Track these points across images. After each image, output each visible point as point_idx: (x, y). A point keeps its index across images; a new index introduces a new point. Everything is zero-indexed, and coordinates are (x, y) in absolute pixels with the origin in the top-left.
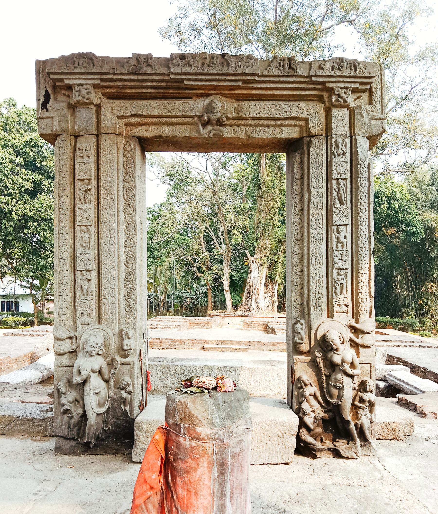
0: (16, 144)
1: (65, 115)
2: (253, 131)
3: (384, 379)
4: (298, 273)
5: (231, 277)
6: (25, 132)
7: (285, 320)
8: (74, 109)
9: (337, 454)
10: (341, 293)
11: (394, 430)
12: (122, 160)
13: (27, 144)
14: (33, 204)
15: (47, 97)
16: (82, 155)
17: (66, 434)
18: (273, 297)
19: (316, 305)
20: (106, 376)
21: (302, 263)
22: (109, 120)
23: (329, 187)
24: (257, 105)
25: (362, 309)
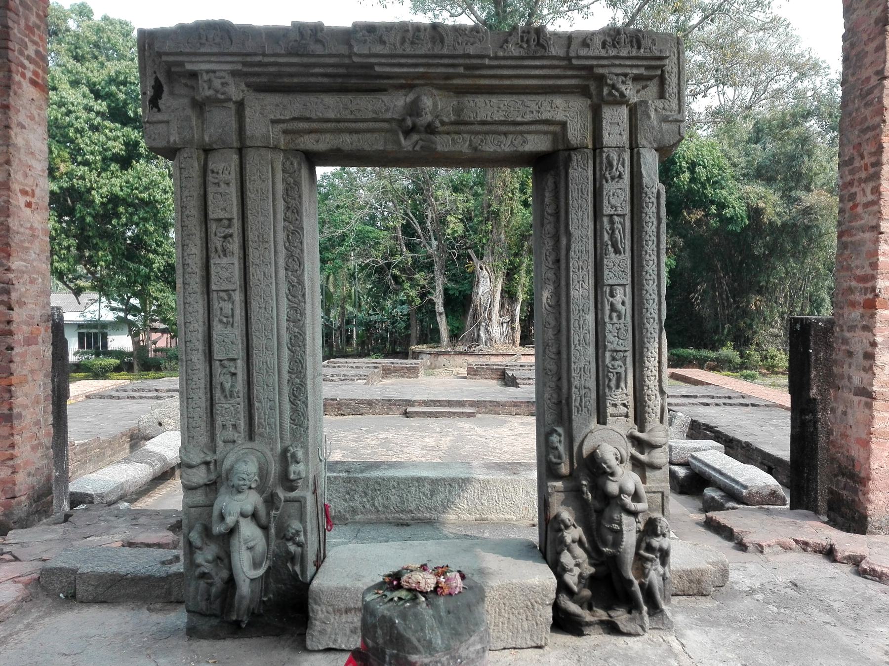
0: (94, 79)
1: (188, 119)
2: (482, 141)
3: (686, 465)
4: (553, 356)
5: (446, 291)
6: (108, 60)
7: (532, 359)
8: (201, 107)
9: (612, 628)
10: (618, 387)
11: (699, 582)
12: (280, 187)
13: (112, 81)
14: (125, 177)
15: (158, 89)
16: (216, 181)
17: (204, 609)
18: (512, 323)
19: (580, 405)
22: (258, 125)
23: (598, 227)
24: (488, 102)
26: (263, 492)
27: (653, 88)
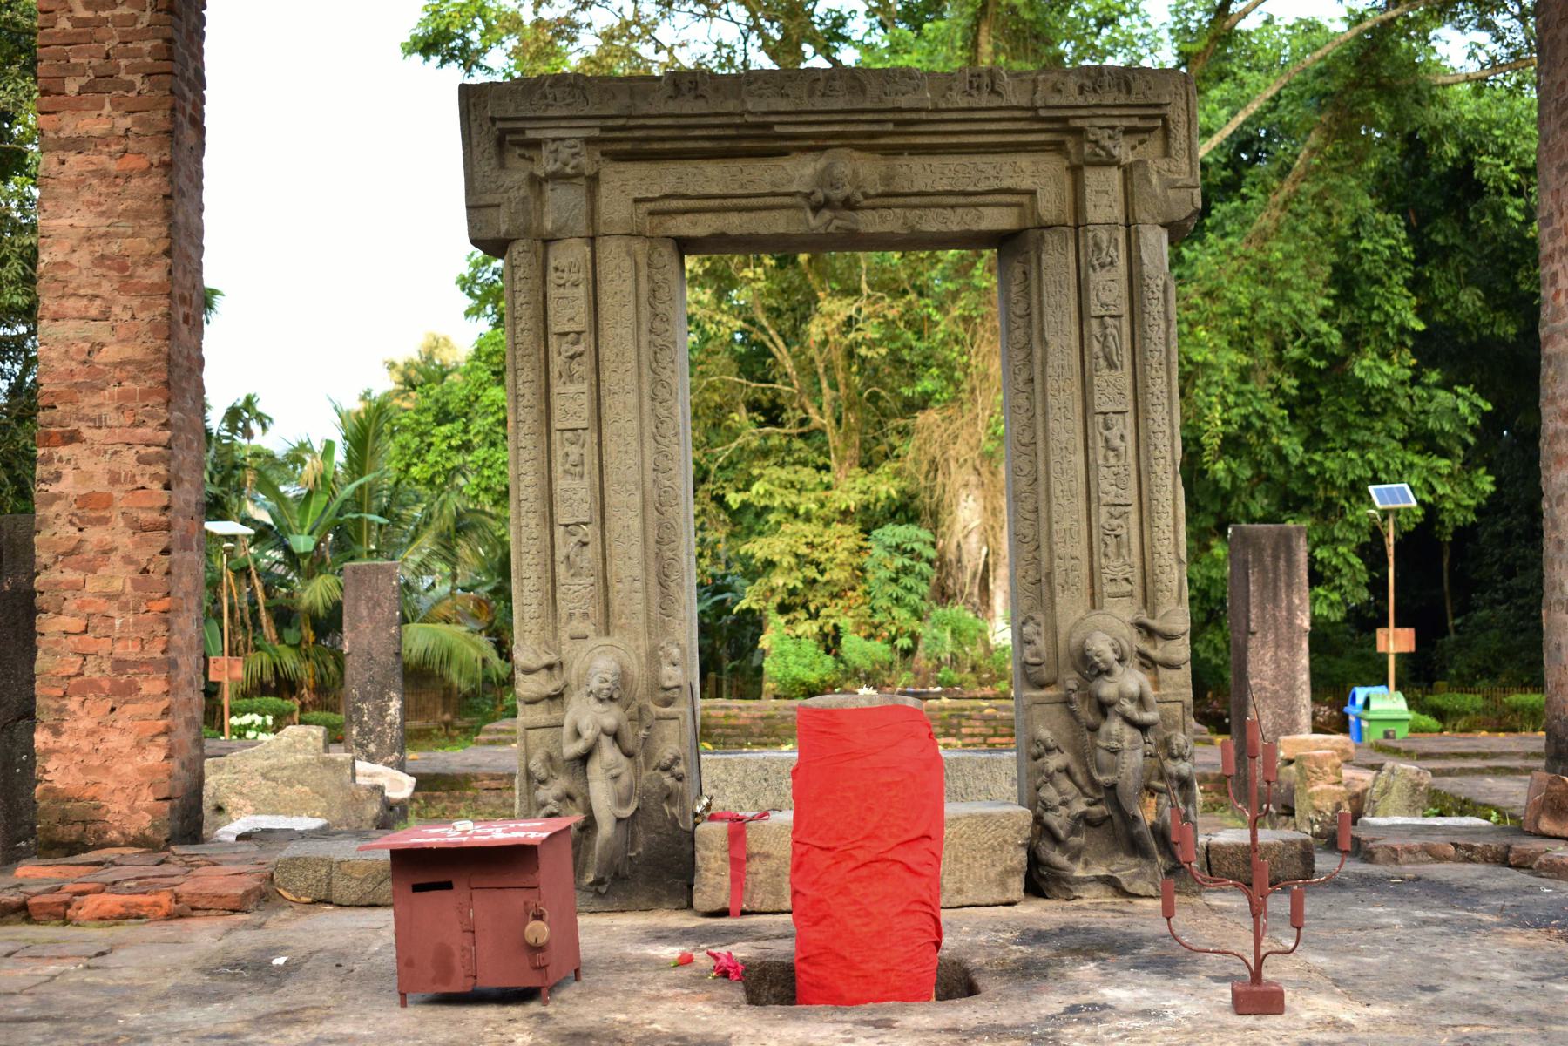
4: (1028, 516)
20: (630, 745)
21: (1035, 492)
26: (628, 706)
27: (1154, 145)
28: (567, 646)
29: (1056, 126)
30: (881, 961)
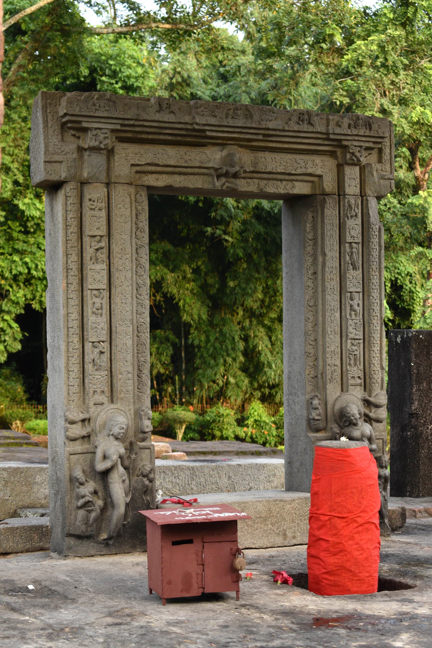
4: (312, 343)
16: (93, 207)
25: (375, 381)
28: (93, 409)
29: (335, 143)
30: (368, 572)
